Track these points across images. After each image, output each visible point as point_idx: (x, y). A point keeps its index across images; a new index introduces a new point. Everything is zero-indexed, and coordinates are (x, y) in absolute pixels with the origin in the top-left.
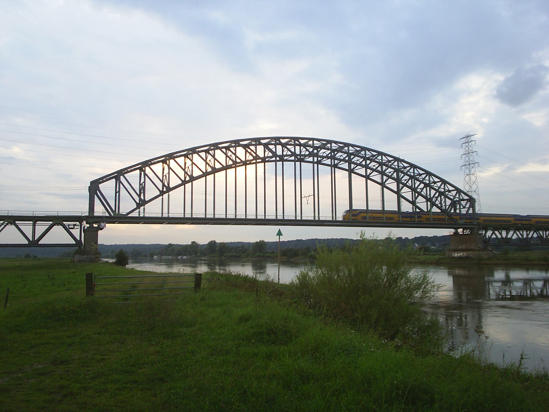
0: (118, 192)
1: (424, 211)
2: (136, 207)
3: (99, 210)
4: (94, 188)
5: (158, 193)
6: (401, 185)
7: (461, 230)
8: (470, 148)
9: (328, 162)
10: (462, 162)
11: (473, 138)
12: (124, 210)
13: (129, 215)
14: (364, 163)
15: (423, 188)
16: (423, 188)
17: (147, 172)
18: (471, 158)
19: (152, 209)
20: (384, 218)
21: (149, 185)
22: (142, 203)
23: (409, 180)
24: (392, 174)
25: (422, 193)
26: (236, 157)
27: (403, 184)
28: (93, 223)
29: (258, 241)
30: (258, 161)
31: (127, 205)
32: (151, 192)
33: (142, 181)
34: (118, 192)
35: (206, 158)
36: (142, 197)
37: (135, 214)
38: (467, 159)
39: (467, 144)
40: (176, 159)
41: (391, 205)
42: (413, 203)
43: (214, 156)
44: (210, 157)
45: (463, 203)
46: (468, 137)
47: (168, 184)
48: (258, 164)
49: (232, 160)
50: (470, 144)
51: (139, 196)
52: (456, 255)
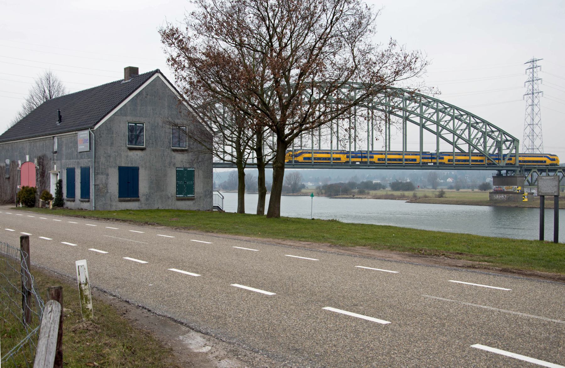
1: (465, 152)
6: (440, 128)
7: (505, 171)
8: (535, 75)
9: (400, 113)
10: (525, 91)
11: (538, 63)
14: (435, 118)
15: (465, 129)
16: (465, 129)
18: (535, 87)
23: (434, 113)
24: (416, 110)
25: (463, 136)
27: (441, 126)
38: (531, 87)
39: (531, 70)
41: (430, 147)
42: (454, 144)
45: (508, 143)
49: (485, 139)
50: (535, 70)
52: (497, 196)
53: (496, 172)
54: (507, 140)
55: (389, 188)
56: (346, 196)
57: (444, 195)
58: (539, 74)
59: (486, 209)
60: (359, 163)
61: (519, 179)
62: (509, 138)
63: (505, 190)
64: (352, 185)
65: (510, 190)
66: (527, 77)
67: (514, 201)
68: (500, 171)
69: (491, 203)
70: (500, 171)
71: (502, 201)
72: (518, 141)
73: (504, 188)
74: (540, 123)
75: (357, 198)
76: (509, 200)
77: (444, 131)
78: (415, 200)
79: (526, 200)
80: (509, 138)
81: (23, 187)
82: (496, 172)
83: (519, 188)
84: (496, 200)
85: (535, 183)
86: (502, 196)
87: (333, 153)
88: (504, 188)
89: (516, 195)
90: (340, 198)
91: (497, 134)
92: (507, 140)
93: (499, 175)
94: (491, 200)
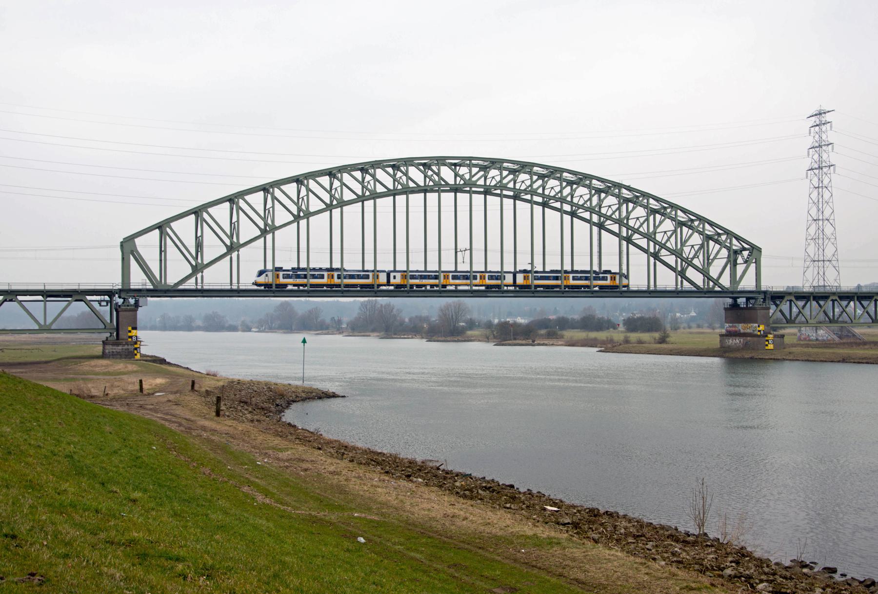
0: (162, 251)
2: (190, 271)
3: (138, 279)
4: (128, 247)
5: (258, 233)
7: (744, 300)
11: (828, 117)
12: (172, 279)
13: (181, 287)
17: (345, 181)
18: (825, 156)
19: (216, 277)
20: (609, 278)
21: (209, 238)
22: (197, 269)
26: (409, 178)
28: (124, 303)
29: (419, 459)
30: (505, 192)
31: (177, 271)
32: (213, 247)
33: (234, 219)
34: (162, 251)
35: (363, 179)
36: (235, 239)
37: (190, 284)
38: (816, 157)
40: (282, 187)
43: (341, 181)
44: (368, 178)
46: (820, 114)
47: (273, 221)
48: (442, 194)
50: (824, 128)
51: (264, 219)
53: (730, 301)
54: (744, 249)
55: (622, 328)
56: (524, 342)
57: (668, 339)
58: (830, 136)
59: (716, 360)
60: (597, 289)
61: (760, 313)
62: (746, 246)
63: (742, 331)
64: (544, 324)
65: (748, 331)
66: (810, 141)
67: (753, 349)
68: (735, 299)
69: (721, 352)
70: (735, 299)
71: (737, 349)
72: (759, 250)
73: (741, 327)
74: (832, 217)
75: (539, 345)
76: (746, 346)
77: (636, 236)
78: (610, 347)
79: (771, 347)
80: (746, 246)
81: (624, 324)
82: (730, 301)
83: (762, 328)
84: (729, 347)
85: (796, 318)
86: (738, 341)
87: (345, 278)
88: (741, 327)
89: (755, 339)
90: (510, 345)
91: (724, 237)
92: (744, 249)
93: (735, 306)
94: (722, 347)
